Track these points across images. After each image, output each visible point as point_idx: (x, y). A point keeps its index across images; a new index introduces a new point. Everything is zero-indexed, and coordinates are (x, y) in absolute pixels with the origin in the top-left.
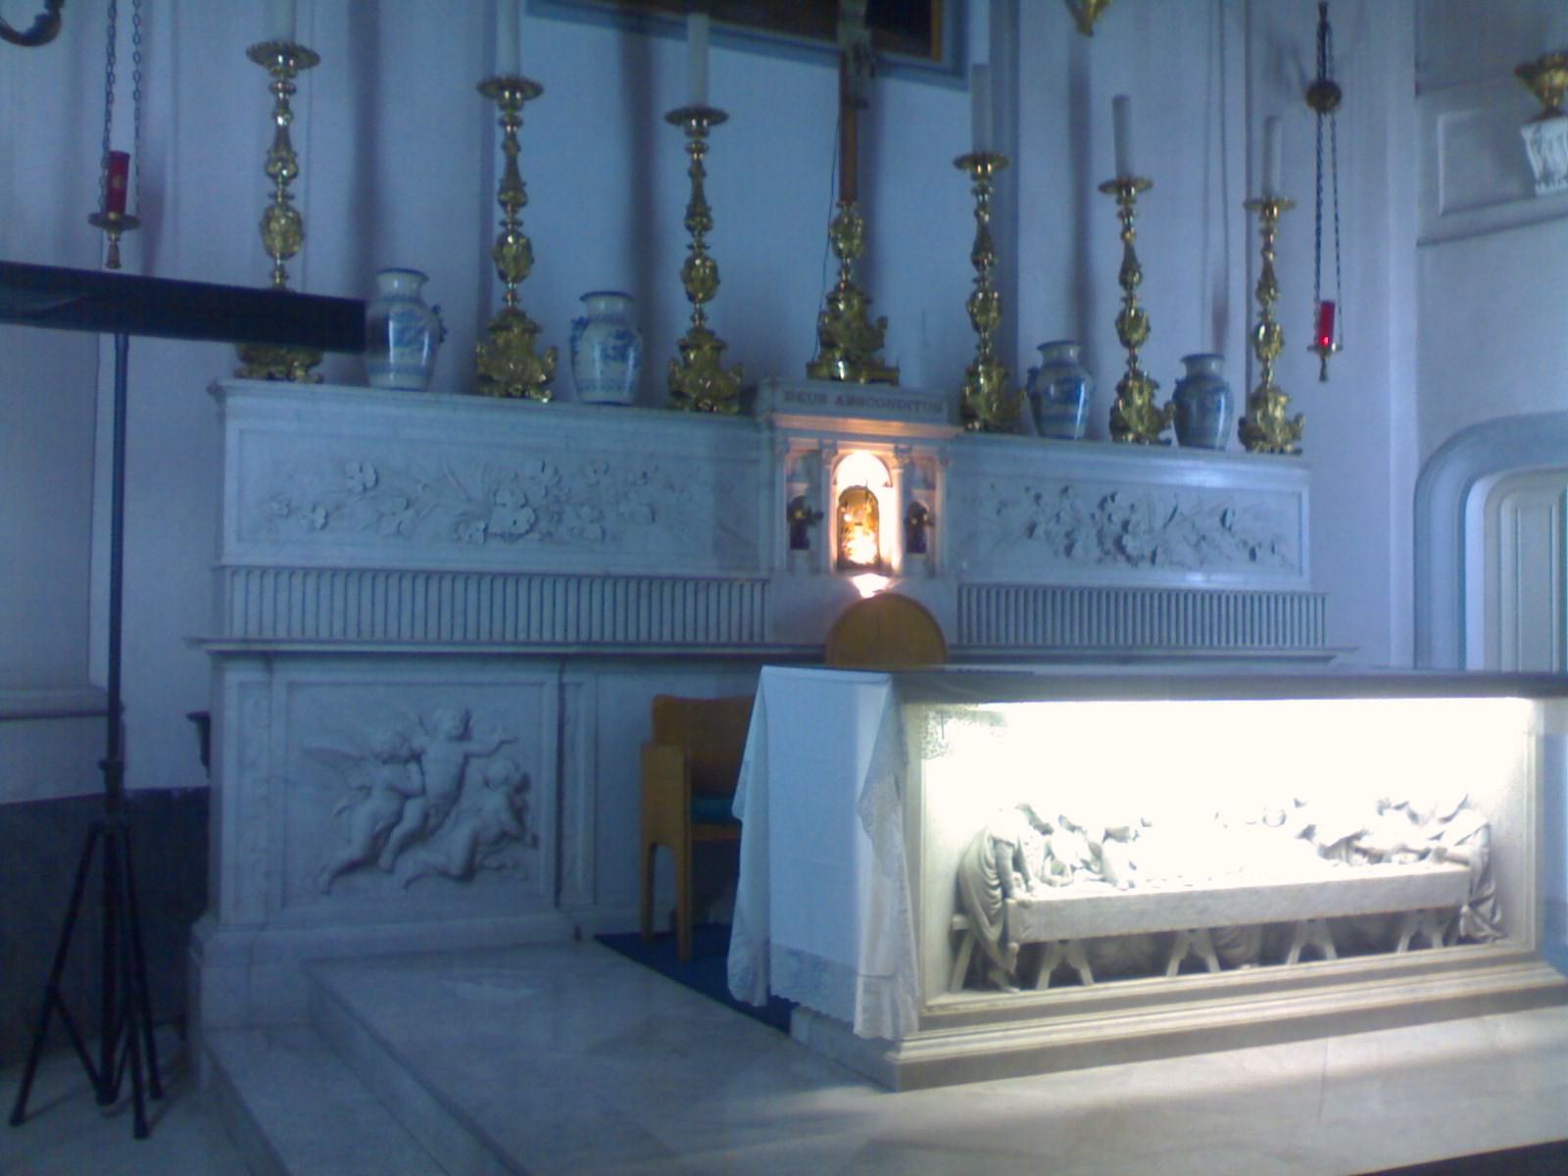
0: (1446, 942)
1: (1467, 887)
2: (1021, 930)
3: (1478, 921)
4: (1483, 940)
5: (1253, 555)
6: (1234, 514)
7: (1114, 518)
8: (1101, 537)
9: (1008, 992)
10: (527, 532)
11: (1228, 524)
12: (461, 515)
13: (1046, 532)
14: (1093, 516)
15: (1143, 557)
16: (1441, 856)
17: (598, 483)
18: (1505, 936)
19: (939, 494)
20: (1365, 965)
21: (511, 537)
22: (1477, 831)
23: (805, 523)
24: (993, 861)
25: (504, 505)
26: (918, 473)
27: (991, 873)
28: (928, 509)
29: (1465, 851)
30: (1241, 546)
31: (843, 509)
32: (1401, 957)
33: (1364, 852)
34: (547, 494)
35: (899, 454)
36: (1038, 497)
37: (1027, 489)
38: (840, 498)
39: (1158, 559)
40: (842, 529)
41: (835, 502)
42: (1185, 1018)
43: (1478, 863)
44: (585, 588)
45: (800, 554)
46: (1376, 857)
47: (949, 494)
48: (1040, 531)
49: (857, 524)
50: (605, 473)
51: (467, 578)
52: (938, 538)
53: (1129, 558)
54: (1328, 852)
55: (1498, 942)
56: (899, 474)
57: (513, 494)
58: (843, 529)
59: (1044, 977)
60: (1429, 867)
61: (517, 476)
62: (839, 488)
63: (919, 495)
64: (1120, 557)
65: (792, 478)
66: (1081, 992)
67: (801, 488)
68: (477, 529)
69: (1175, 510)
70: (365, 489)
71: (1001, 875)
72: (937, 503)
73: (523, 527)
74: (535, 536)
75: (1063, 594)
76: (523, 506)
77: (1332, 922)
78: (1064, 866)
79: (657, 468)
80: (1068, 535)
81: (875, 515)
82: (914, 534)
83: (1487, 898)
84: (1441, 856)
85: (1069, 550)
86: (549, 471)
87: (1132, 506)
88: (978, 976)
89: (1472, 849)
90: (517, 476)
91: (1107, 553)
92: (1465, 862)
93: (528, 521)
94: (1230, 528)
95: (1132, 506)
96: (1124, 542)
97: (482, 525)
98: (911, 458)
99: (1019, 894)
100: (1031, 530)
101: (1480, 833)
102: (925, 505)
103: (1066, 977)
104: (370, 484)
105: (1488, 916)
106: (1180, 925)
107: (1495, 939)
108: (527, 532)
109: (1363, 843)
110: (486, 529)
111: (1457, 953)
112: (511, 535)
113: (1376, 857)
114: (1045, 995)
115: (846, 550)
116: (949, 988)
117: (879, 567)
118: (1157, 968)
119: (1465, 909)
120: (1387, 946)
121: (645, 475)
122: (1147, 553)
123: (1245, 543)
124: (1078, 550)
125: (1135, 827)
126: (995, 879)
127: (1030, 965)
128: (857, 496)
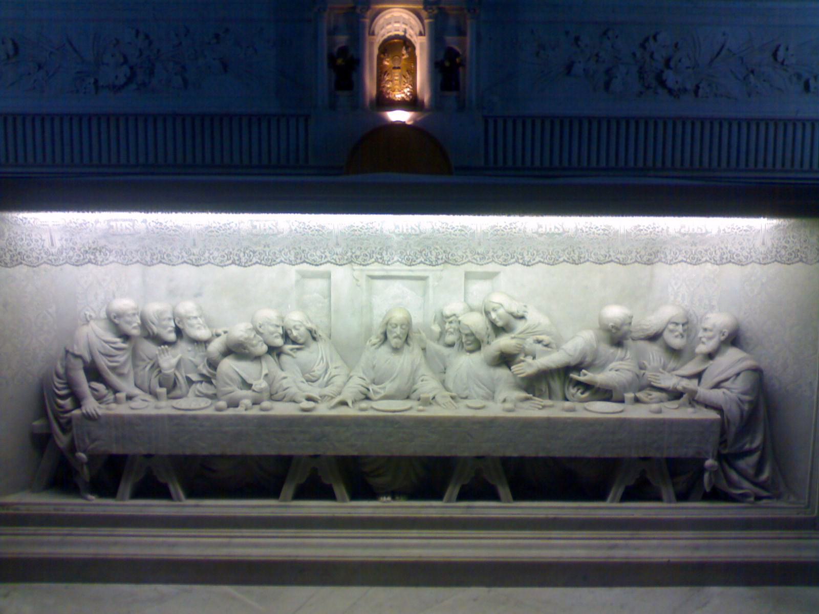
0: (682, 497)
1: (715, 438)
2: (87, 441)
3: (734, 476)
4: (742, 498)
5: (807, 87)
6: (787, 49)
7: (656, 56)
8: (641, 72)
9: (86, 499)
10: (126, 84)
11: (780, 59)
12: (78, 72)
13: (584, 70)
14: (634, 54)
15: (685, 90)
16: (694, 401)
17: (180, 44)
18: (778, 497)
19: (469, 39)
20: (334, 510)
21: (116, 89)
22: (738, 374)
23: (347, 68)
24: (61, 371)
25: (107, 64)
26: (452, 22)
27: (58, 383)
28: (461, 53)
29: (717, 396)
30: (794, 79)
31: (382, 56)
32: (610, 508)
33: (586, 386)
34: (141, 54)
35: (428, 7)
36: (577, 39)
37: (567, 33)
38: (380, 49)
39: (701, 91)
40: (381, 72)
41: (376, 52)
42: (367, 546)
43: (733, 412)
44: (160, 125)
45: (343, 95)
46: (605, 393)
47: (479, 38)
48: (578, 68)
49: (394, 68)
50: (186, 35)
51: (71, 119)
52: (470, 78)
53: (670, 91)
54: (535, 384)
55: (763, 502)
56: (430, 23)
57: (113, 56)
58: (382, 72)
59: (126, 487)
60: (674, 412)
61: (118, 41)
62: (379, 40)
63: (451, 40)
64: (660, 90)
65: (333, 32)
66: (167, 506)
67: (342, 39)
68: (90, 83)
69: (723, 47)
70: (8, 56)
71: (70, 384)
72: (467, 46)
73: (122, 80)
74: (133, 86)
75: (646, 123)
76: (122, 64)
77: (505, 461)
78: (264, 379)
79: (227, 30)
80: (608, 71)
81: (413, 58)
82: (446, 69)
83: (750, 452)
84: (694, 401)
85: (607, 86)
86: (141, 37)
87: (676, 45)
88: (63, 478)
89: (731, 396)
90: (118, 41)
91: (648, 87)
92: (718, 409)
93: (125, 75)
94: (782, 63)
95: (676, 45)
96: (664, 77)
97: (92, 80)
98: (441, 9)
99: (91, 405)
100: (569, 68)
101: (741, 376)
102: (457, 48)
103: (151, 488)
104: (11, 53)
105: (751, 472)
106: (464, 451)
107: (758, 498)
108: (126, 84)
109: (586, 376)
110: (96, 82)
111: (696, 509)
112: (114, 86)
113: (605, 393)
114: (125, 505)
115: (385, 90)
116: (30, 486)
117: (412, 104)
118: (271, 491)
119: (709, 462)
120: (598, 493)
121: (217, 36)
122: (690, 86)
123: (799, 76)
124: (616, 84)
125: (554, 346)
126: (64, 389)
127: (109, 474)
128: (397, 45)
